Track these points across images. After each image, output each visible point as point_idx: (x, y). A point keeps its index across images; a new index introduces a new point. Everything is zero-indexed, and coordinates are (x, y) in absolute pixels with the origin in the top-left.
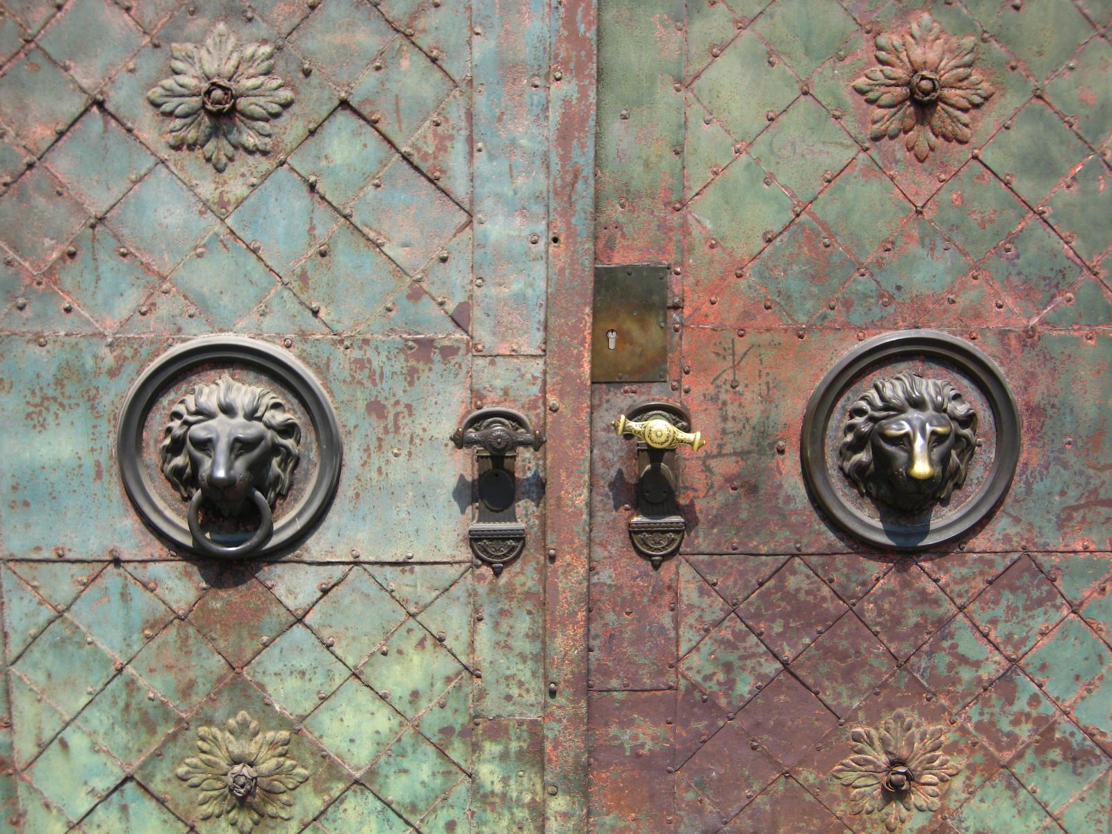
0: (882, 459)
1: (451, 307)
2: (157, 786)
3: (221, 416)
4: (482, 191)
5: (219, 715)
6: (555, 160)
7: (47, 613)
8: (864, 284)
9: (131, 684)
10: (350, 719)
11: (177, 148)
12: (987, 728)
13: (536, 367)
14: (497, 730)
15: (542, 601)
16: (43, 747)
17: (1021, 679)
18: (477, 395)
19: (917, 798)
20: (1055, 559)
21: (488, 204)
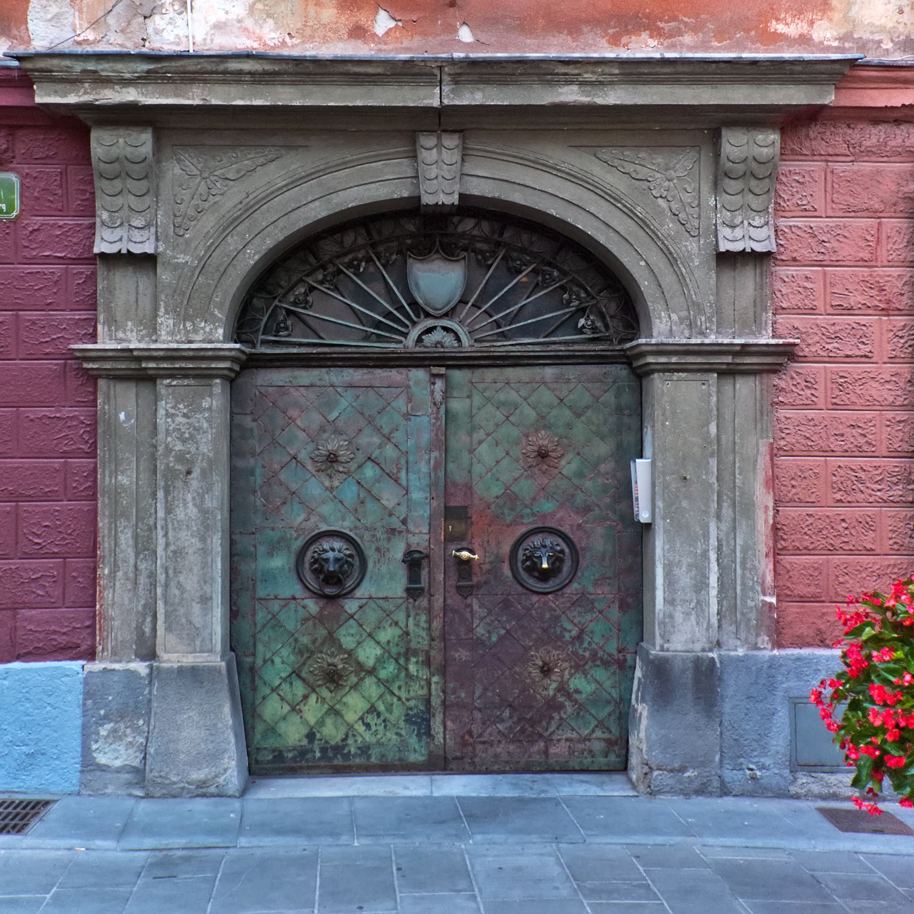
0: (534, 563)
1: (401, 518)
2: (303, 674)
3: (331, 552)
4: (411, 484)
5: (325, 650)
6: (432, 475)
7: (270, 616)
8: (528, 511)
9: (296, 640)
10: (368, 650)
11: (318, 471)
12: (575, 653)
13: (427, 537)
14: (415, 653)
15: (429, 611)
16: (265, 661)
17: (585, 636)
18: (408, 545)
19: (553, 678)
20: (592, 597)
21: (412, 488)
